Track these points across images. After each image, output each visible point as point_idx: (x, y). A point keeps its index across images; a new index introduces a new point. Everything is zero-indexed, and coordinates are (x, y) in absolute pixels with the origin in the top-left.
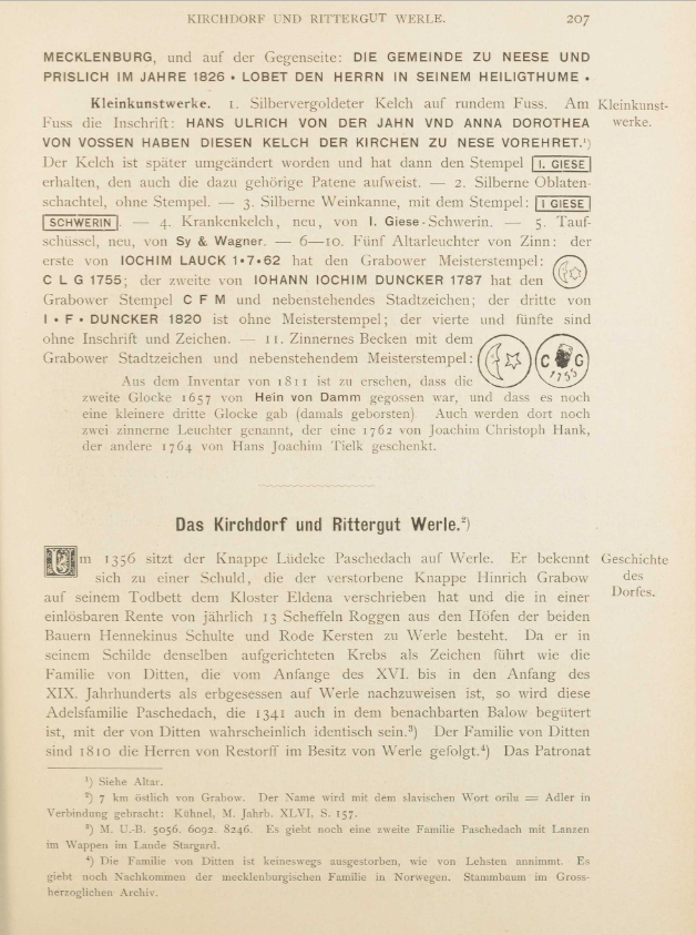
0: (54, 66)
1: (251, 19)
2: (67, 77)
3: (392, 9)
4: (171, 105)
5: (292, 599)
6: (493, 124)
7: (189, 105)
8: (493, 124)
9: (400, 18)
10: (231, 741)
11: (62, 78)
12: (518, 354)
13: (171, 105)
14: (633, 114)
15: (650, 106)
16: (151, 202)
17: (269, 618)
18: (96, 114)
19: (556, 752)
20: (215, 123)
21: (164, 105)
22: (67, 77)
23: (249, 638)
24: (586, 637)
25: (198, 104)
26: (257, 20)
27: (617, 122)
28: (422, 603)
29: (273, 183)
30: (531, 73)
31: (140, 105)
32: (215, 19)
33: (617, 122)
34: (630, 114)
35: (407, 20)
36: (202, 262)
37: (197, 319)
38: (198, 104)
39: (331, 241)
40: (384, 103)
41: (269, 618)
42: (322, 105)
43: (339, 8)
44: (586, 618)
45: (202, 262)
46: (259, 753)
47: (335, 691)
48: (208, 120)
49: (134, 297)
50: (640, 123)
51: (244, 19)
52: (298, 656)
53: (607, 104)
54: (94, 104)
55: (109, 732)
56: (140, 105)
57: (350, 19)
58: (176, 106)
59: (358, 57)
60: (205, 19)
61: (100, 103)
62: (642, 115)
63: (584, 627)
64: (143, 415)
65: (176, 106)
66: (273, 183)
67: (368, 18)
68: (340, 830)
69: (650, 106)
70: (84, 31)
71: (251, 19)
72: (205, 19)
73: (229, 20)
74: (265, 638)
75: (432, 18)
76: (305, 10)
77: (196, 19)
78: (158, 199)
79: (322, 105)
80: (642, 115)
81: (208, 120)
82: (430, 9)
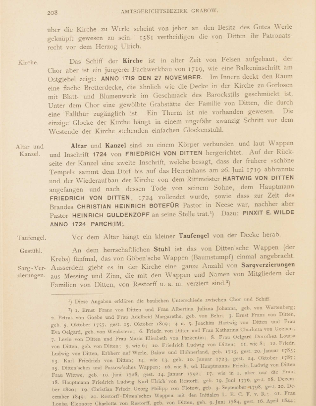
0: (54, 194)
2: (93, 207)
6: (227, 179)
8: (227, 179)
10: (80, 159)
11: (91, 207)
12: (152, 199)
16: (178, 214)
17: (54, 361)
19: (272, 36)
22: (93, 207)
28: (143, 191)
30: (160, 204)
36: (113, 216)
37: (117, 78)
39: (256, 170)
41: (54, 361)
45: (113, 216)
46: (148, 285)
48: (55, 223)
49: (185, 213)
52: (170, 96)
59: (273, 178)
64: (282, 161)
74: (140, 146)
78: (180, 213)
81: (55, 223)
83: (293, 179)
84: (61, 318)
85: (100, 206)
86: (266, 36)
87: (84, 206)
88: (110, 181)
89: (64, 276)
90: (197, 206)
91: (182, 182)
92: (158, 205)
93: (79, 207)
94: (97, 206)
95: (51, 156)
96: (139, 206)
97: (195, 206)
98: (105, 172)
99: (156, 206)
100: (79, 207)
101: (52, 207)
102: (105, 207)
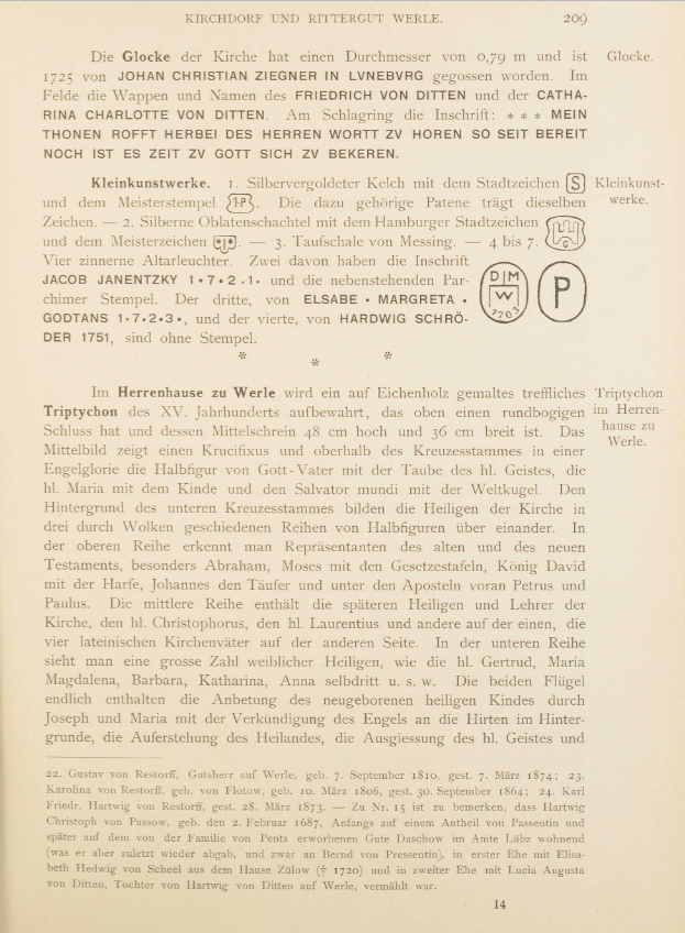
1: (248, 18)
2: (207, 76)
3: (389, 9)
4: (171, 184)
5: (368, 721)
7: (189, 185)
9: (398, 18)
11: (202, 76)
13: (171, 184)
14: (630, 193)
15: (646, 184)
18: (99, 194)
20: (100, 319)
21: (164, 184)
23: (391, 625)
24: (581, 510)
25: (198, 184)
26: (255, 19)
27: (613, 200)
29: (384, 204)
30: (559, 91)
31: (140, 185)
32: (214, 19)
33: (613, 200)
34: (627, 192)
35: (405, 19)
37: (486, 134)
38: (198, 184)
40: (376, 183)
42: (319, 185)
43: (339, 8)
44: (582, 491)
47: (486, 487)
48: (116, 277)
50: (637, 201)
51: (241, 19)
53: (604, 182)
54: (95, 183)
55: (366, 567)
56: (140, 185)
57: (348, 18)
58: (176, 185)
60: (202, 19)
61: (101, 182)
62: (639, 192)
63: (580, 500)
65: (176, 185)
66: (384, 204)
67: (366, 17)
68: (405, 886)
69: (646, 184)
70: (194, 8)
71: (248, 18)
72: (202, 19)
73: (227, 20)
75: (429, 18)
76: (302, 9)
77: (194, 18)
79: (319, 185)
80: (639, 192)
81: (116, 277)
82: (427, 9)
83: (460, 137)
84: (432, 204)
85: (223, 75)
86: (434, 203)
87: (100, 112)
88: (315, 414)
89: (130, 718)
90: (339, 491)
91: (522, 62)
92: (74, 317)
93: (90, 115)
94: (217, 75)
95: (540, 58)
96: (278, 154)
97: (191, 624)
98: (268, 490)
99: (229, 154)
100: (90, 115)
101: (580, 809)
102: (233, 76)
